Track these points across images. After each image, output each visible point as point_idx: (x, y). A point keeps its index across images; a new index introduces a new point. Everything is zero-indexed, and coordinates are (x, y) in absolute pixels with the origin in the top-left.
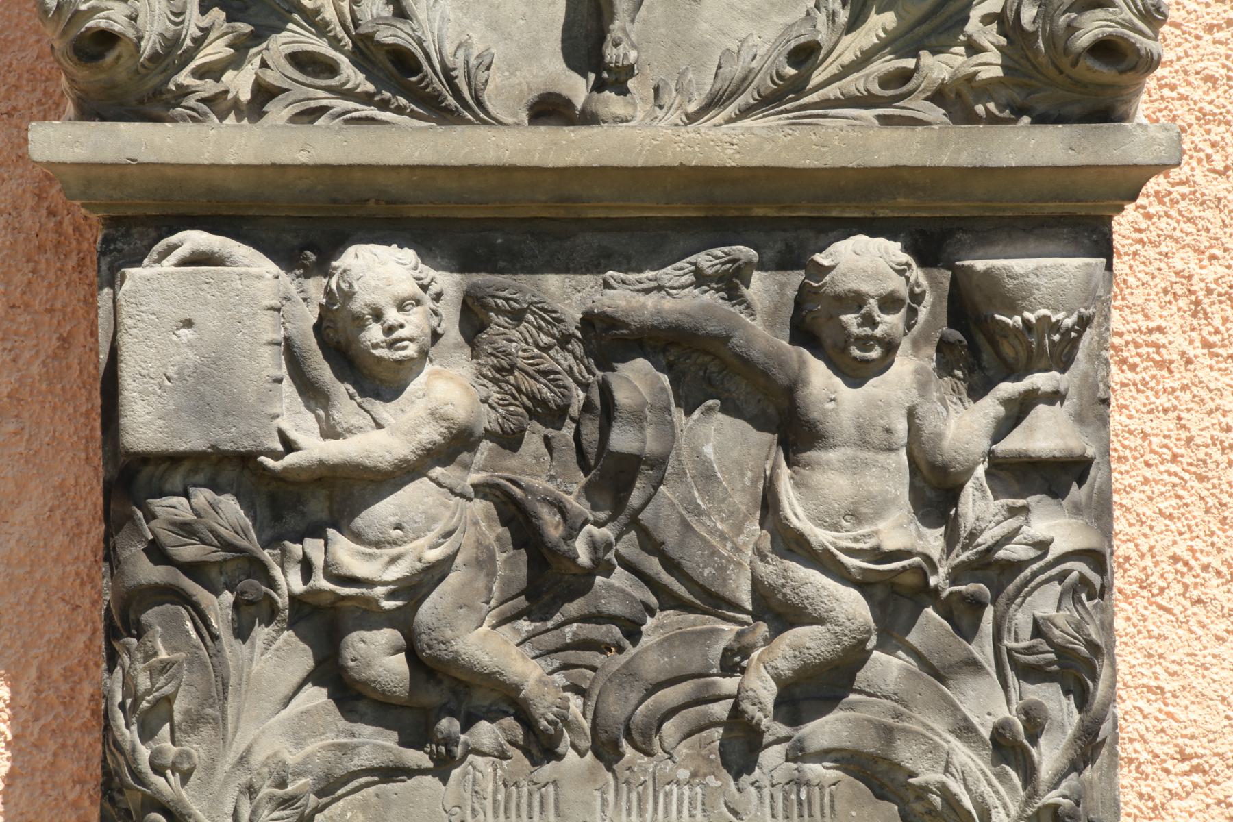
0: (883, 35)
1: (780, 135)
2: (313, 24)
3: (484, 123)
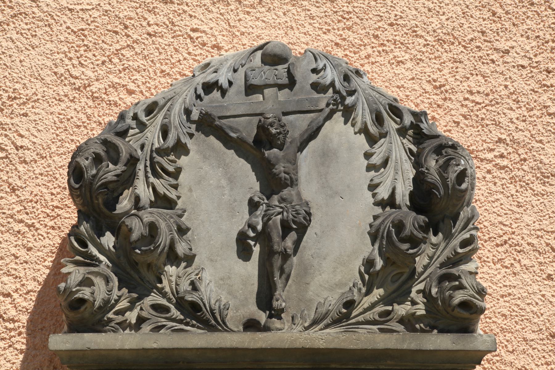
0: (379, 297)
1: (341, 336)
2: (161, 293)
3: (226, 331)
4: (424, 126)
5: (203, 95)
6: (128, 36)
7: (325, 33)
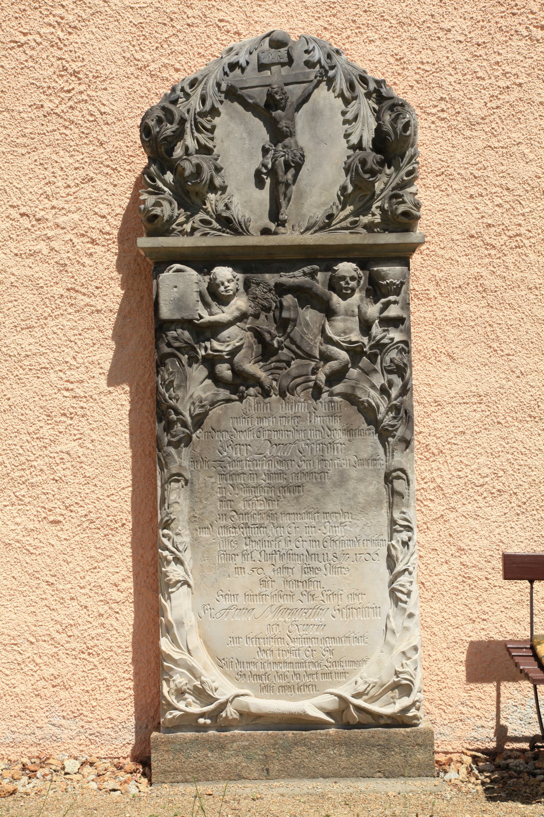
4: (383, 90)
5: (228, 72)
6: (173, 27)
7: (316, 20)
